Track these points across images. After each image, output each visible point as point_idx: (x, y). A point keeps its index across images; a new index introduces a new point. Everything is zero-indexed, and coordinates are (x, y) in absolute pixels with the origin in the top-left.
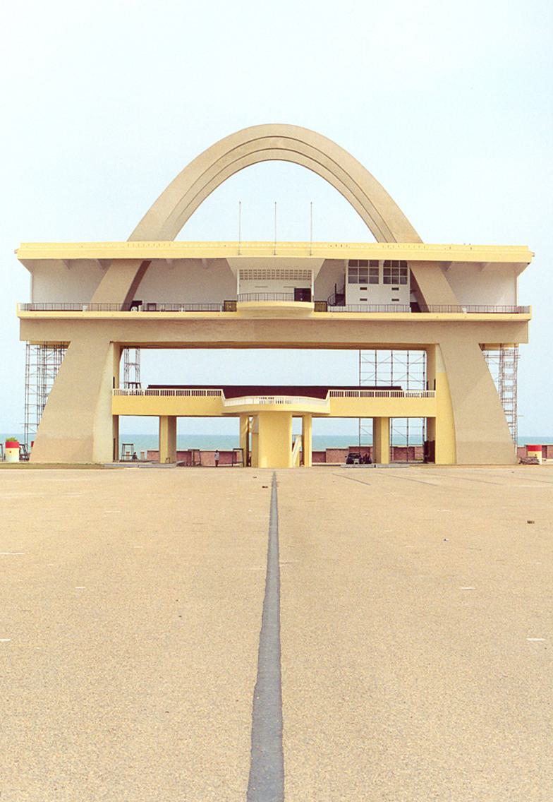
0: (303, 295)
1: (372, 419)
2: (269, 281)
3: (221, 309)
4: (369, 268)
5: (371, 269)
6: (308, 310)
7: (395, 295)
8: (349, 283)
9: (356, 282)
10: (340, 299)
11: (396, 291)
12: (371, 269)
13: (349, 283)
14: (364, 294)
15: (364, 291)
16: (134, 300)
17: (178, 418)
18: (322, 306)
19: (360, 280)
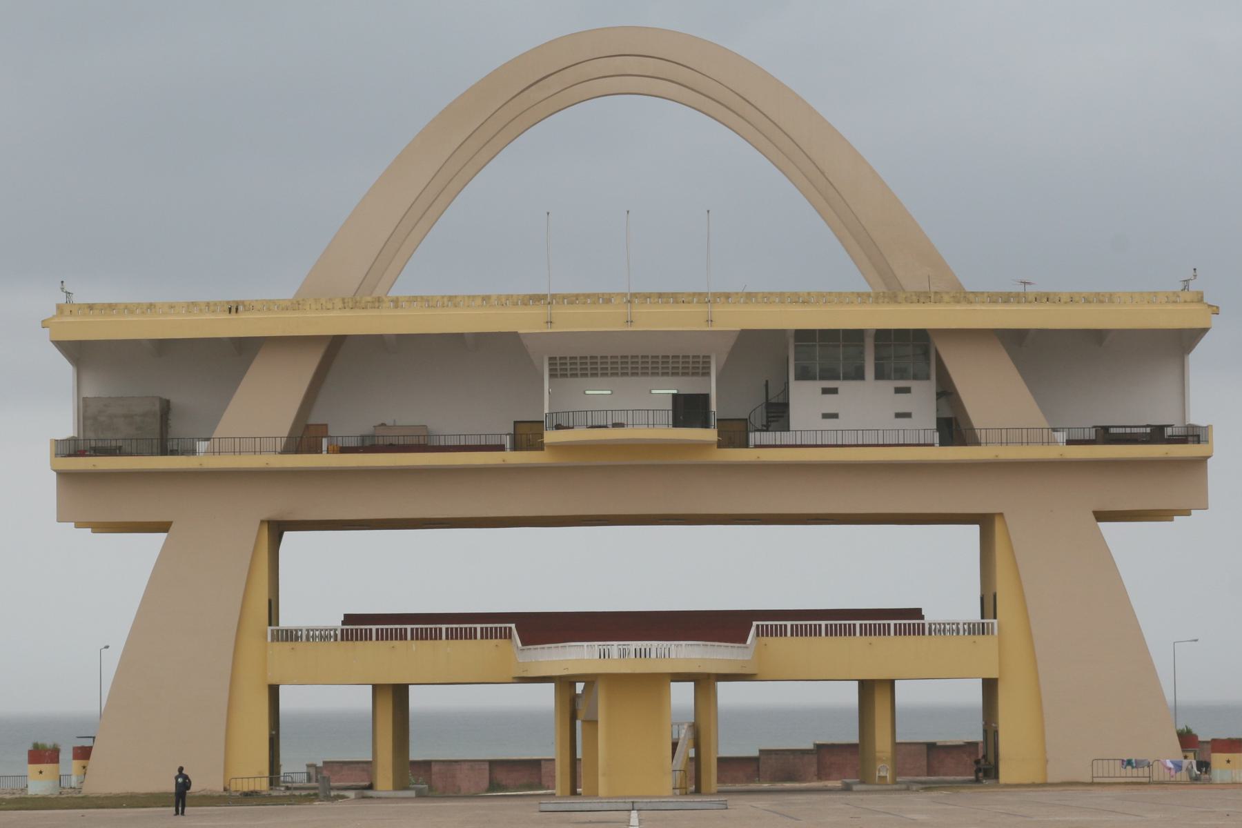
6: (701, 446)
7: (903, 403)
9: (813, 378)
14: (830, 403)
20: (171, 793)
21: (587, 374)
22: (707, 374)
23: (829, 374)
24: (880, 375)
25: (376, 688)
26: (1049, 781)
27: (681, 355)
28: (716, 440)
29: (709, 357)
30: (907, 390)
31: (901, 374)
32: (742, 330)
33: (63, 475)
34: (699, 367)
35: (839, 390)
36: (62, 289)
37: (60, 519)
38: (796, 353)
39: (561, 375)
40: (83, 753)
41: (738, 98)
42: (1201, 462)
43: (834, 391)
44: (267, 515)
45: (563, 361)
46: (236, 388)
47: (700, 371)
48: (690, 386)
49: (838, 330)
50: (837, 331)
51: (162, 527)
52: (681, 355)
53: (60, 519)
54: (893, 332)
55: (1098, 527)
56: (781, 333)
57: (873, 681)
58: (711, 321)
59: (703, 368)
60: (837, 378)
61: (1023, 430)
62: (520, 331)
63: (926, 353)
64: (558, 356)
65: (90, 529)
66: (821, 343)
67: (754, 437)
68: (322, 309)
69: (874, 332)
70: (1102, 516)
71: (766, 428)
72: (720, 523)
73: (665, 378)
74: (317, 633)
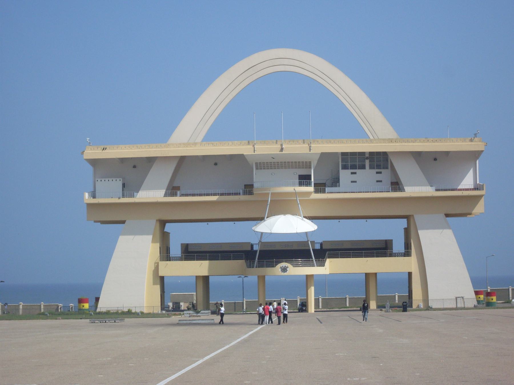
0: (304, 180)
1: (365, 274)
2: (247, 196)
3: (241, 192)
4: (349, 157)
5: (350, 157)
6: (309, 193)
7: (379, 177)
8: (342, 169)
9: (348, 169)
10: (335, 182)
11: (380, 174)
12: (350, 157)
13: (342, 169)
14: (354, 177)
15: (378, 180)
16: (174, 185)
17: (210, 276)
18: (320, 187)
19: (377, 166)
20: (371, 300)
21: (286, 168)
22: (310, 168)
23: (353, 167)
24: (371, 167)
25: (258, 277)
26: (466, 306)
27: (287, 162)
28: (313, 191)
29: (311, 162)
30: (380, 173)
31: (379, 167)
32: (322, 153)
34: (308, 165)
39: (277, 168)
40: (190, 302)
43: (355, 173)
44: (158, 218)
45: (271, 164)
47: (298, 167)
48: (304, 172)
50: (356, 152)
52: (287, 162)
55: (405, 218)
56: (336, 154)
57: (369, 273)
59: (274, 166)
60: (356, 169)
61: (470, 185)
62: (244, 154)
63: (387, 160)
64: (280, 162)
65: (100, 223)
66: (359, 157)
67: (327, 189)
68: (412, 142)
69: (369, 153)
70: (447, 215)
71: (332, 186)
72: (175, 222)
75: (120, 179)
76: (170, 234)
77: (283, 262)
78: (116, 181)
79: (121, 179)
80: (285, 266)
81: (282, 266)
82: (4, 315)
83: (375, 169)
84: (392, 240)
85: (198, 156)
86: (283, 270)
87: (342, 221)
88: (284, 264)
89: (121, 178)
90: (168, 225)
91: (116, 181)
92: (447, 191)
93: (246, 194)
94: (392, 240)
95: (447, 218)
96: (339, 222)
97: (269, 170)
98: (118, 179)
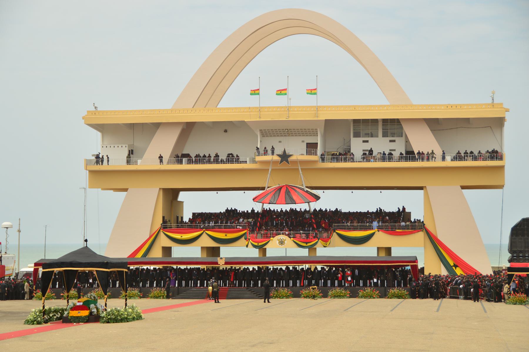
20: (32, 271)
24: (385, 135)
29: (317, 129)
31: (393, 135)
33: (91, 172)
35: (369, 141)
36: (94, 105)
37: (410, 213)
38: (354, 127)
41: (255, 55)
42: (502, 167)
46: (152, 139)
48: (311, 140)
49: (388, 119)
50: (360, 120)
51: (126, 190)
52: (296, 129)
53: (410, 213)
54: (396, 120)
58: (317, 116)
70: (463, 187)
73: (311, 137)
74: (523, 283)
75: (126, 145)
76: (184, 203)
77: (279, 234)
78: (122, 147)
79: (127, 146)
80: (283, 238)
81: (279, 238)
82: (220, 288)
83: (361, 137)
84: (410, 213)
85: (347, 119)
86: (280, 243)
87: (220, 192)
88: (282, 237)
89: (126, 144)
90: (181, 193)
91: (122, 147)
92: (198, 165)
93: (199, 163)
94: (410, 213)
95: (462, 190)
96: (244, 193)
97: (264, 138)
98: (124, 146)
